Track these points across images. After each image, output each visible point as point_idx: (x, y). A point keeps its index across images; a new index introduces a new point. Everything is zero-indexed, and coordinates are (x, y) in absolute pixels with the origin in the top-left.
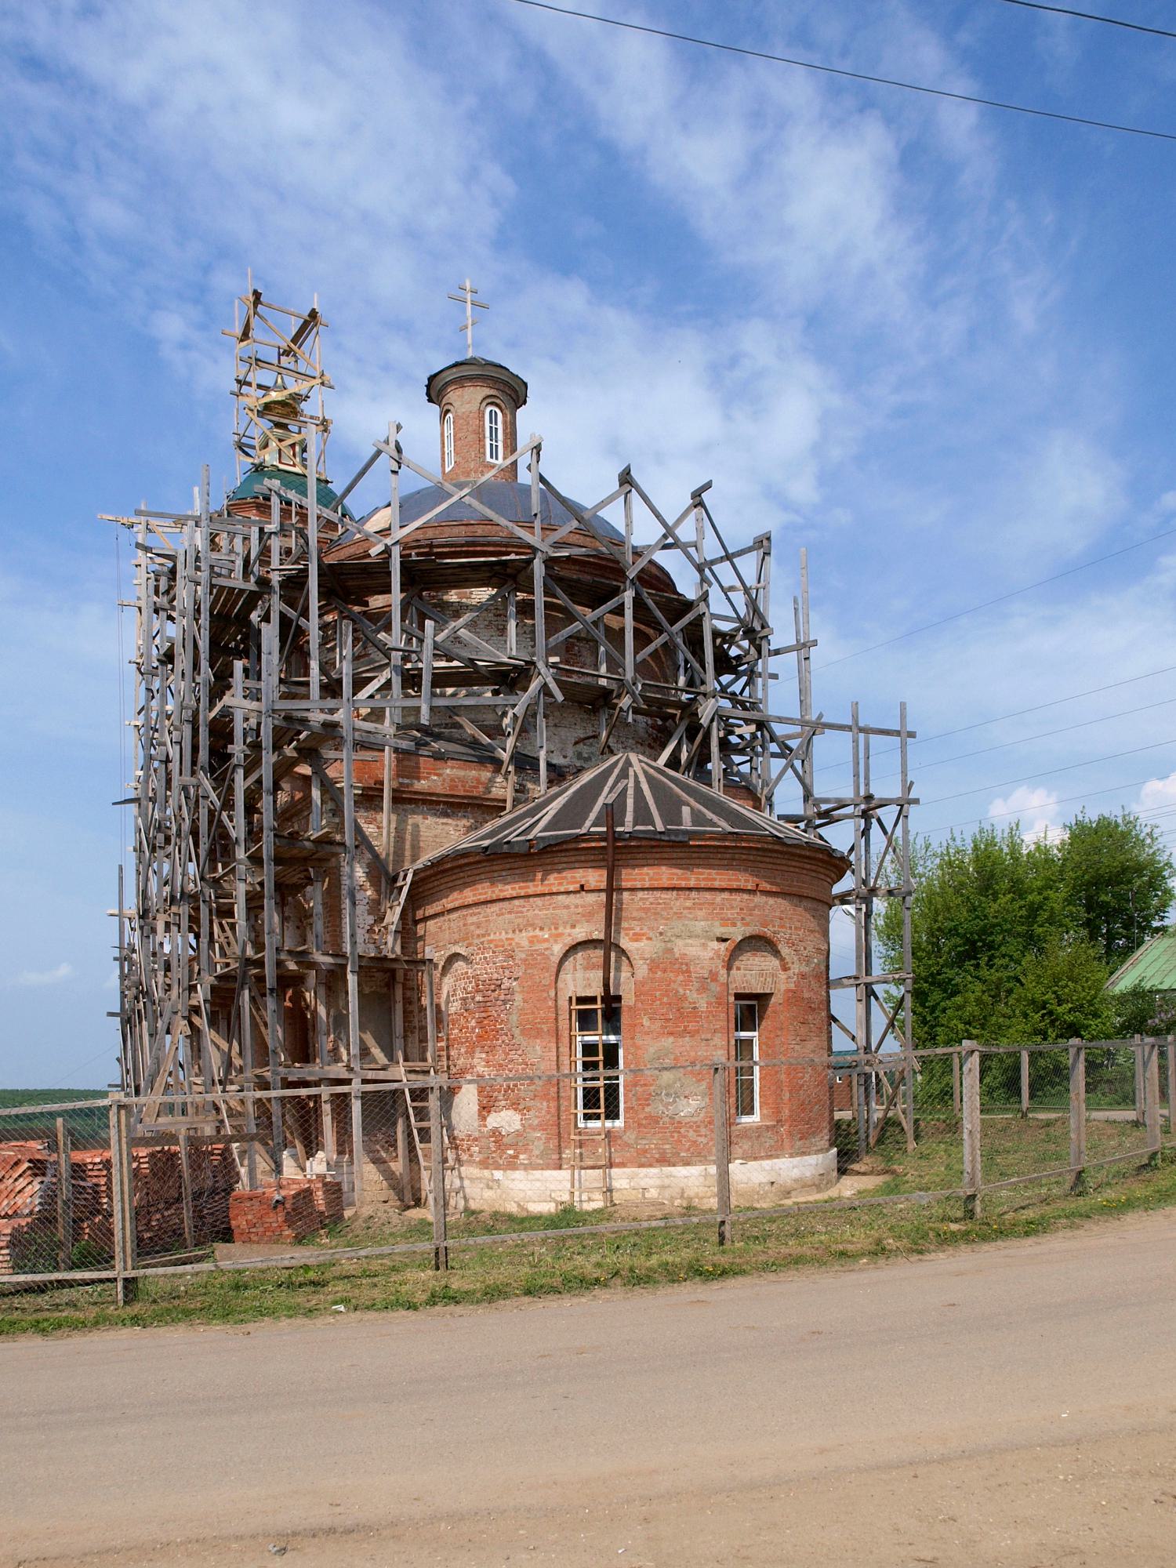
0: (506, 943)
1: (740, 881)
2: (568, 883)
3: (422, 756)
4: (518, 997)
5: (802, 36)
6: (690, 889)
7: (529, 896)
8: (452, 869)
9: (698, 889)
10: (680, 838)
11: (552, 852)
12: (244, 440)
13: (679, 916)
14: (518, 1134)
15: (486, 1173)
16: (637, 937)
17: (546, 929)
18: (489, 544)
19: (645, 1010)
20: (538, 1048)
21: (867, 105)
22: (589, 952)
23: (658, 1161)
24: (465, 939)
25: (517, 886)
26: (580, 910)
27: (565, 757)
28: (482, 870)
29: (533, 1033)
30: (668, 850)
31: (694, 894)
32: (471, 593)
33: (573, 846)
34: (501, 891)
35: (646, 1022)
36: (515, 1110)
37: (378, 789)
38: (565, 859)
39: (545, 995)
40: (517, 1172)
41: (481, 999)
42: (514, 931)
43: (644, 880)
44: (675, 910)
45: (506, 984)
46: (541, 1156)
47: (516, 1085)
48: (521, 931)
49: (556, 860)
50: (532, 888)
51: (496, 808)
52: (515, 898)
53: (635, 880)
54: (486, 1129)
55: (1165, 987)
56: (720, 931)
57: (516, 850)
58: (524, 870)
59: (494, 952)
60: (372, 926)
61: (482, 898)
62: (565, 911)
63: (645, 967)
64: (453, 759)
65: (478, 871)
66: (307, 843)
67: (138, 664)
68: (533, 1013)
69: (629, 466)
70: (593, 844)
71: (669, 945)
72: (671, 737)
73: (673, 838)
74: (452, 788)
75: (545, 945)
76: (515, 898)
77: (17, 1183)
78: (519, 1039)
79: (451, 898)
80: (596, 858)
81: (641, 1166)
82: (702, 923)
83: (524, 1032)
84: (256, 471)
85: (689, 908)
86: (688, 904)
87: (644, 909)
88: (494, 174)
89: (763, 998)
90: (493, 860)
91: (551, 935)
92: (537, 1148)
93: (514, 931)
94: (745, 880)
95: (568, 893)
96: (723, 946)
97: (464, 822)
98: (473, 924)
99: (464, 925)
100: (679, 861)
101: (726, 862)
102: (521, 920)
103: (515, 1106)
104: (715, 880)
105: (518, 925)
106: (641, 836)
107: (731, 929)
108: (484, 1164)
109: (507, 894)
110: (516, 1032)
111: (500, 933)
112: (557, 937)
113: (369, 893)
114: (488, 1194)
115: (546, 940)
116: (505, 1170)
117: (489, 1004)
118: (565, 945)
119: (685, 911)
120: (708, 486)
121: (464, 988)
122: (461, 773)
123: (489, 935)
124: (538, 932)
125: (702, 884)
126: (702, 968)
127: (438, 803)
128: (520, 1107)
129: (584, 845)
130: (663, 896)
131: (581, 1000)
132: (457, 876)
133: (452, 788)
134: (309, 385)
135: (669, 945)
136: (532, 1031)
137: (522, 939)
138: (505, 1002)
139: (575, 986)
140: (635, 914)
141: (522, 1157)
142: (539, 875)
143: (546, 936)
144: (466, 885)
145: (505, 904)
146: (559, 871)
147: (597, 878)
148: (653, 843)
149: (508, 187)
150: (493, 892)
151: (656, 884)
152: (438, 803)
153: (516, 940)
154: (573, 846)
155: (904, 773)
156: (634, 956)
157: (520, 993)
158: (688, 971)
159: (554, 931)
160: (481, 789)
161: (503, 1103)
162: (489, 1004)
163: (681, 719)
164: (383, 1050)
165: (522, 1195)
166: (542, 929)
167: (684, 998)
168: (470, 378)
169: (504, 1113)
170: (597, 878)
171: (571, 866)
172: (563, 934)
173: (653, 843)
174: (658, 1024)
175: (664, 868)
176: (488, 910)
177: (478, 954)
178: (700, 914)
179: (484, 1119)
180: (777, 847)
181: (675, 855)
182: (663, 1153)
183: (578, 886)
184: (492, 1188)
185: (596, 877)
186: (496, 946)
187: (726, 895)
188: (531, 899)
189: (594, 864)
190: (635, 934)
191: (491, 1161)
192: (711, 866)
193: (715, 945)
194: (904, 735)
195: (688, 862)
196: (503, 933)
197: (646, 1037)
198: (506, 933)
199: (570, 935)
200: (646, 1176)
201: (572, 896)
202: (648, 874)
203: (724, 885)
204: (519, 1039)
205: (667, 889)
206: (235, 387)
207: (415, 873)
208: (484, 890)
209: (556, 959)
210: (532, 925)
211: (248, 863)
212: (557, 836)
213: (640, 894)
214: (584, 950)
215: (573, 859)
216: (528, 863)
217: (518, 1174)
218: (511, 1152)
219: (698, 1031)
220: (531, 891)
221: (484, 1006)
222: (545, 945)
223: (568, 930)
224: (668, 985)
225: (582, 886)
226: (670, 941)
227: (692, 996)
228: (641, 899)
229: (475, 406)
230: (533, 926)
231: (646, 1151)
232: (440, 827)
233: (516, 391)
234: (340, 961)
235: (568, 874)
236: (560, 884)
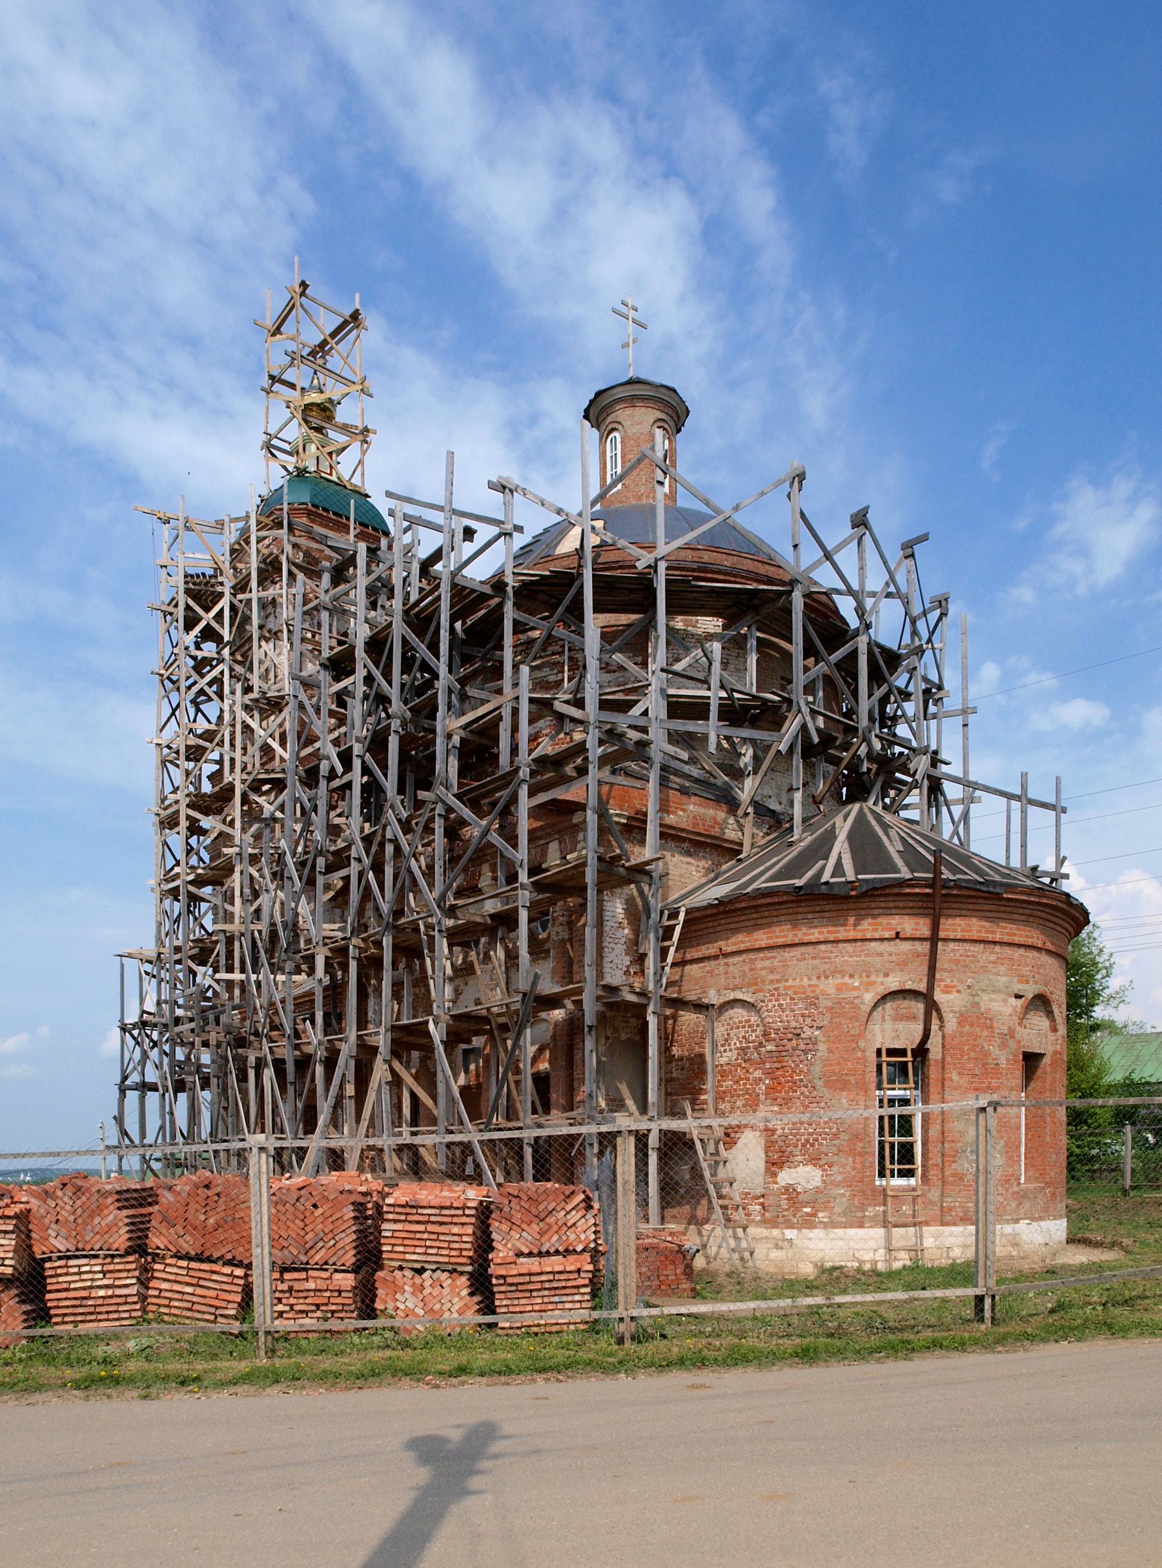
0: (809, 989)
1: (1032, 937)
2: (883, 930)
3: (672, 788)
4: (822, 1047)
5: (609, 93)
6: (994, 943)
7: (837, 941)
8: (744, 908)
9: (1001, 943)
10: (998, 890)
11: (872, 895)
12: (275, 442)
13: (985, 970)
14: (818, 1191)
15: (776, 1232)
16: (947, 990)
17: (856, 976)
18: (719, 572)
19: (954, 1064)
20: (844, 1101)
21: (671, 171)
22: (898, 1002)
23: (962, 1219)
24: (755, 984)
25: (825, 930)
26: (894, 958)
27: (780, 803)
28: (783, 912)
29: (839, 1085)
30: (982, 901)
31: (997, 948)
32: (697, 621)
33: (896, 890)
34: (805, 934)
35: (955, 1077)
36: (815, 1165)
37: (639, 819)
38: (883, 905)
39: (854, 1045)
40: (816, 1231)
41: (774, 1048)
42: (819, 978)
43: (956, 930)
44: (981, 964)
45: (808, 1032)
46: (844, 1214)
47: (817, 1140)
48: (827, 977)
49: (873, 905)
50: (842, 933)
51: (733, 851)
52: (821, 942)
53: (948, 930)
54: (776, 1186)
55: (1153, 1080)
56: (1018, 987)
57: (836, 891)
58: (834, 914)
59: (792, 999)
60: (628, 967)
61: (780, 941)
62: (878, 959)
63: (955, 1020)
64: (695, 795)
65: (779, 913)
66: (621, 870)
67: (162, 675)
68: (839, 1064)
69: (867, 508)
70: (917, 890)
71: (976, 999)
72: (869, 794)
73: (991, 889)
74: (695, 825)
75: (855, 993)
76: (821, 942)
77: (568, 1217)
78: (822, 1090)
79: (730, 941)
80: (916, 904)
81: (943, 1224)
82: (1004, 978)
83: (828, 1084)
84: (298, 476)
85: (994, 963)
86: (993, 958)
87: (954, 960)
88: (291, 186)
89: (1040, 1056)
90: (802, 901)
91: (861, 983)
92: (840, 1206)
93: (819, 978)
94: (1035, 937)
95: (882, 940)
96: (1020, 1002)
97: (703, 863)
98: (763, 968)
99: (751, 970)
100: (988, 914)
101: (1024, 918)
102: (827, 966)
103: (814, 1161)
104: (1015, 935)
105: (824, 971)
106: (964, 885)
107: (1026, 987)
108: (772, 1223)
109: (813, 938)
110: (819, 1083)
111: (802, 980)
112: (868, 985)
113: (626, 931)
114: (775, 1254)
115: (857, 988)
116: (799, 1228)
117: (784, 1054)
118: (877, 993)
119: (991, 965)
120: (924, 538)
121: (744, 1037)
122: (702, 811)
123: (787, 981)
124: (847, 980)
125: (1006, 939)
126: (1003, 1024)
127: (684, 840)
128: (821, 1163)
129: (908, 890)
130: (972, 948)
131: (891, 1052)
132: (750, 916)
133: (695, 825)
134: (346, 390)
135: (976, 999)
136: (838, 1083)
137: (829, 986)
138: (805, 1052)
139: (883, 1038)
140: (946, 966)
141: (820, 1215)
142: (852, 920)
143: (857, 984)
144: (757, 927)
145: (810, 949)
146: (874, 917)
147: (913, 926)
148: (972, 893)
149: (308, 205)
150: (795, 935)
151: (967, 935)
152: (684, 840)
153: (822, 987)
154: (896, 890)
155: (1058, 847)
156: (944, 1009)
157: (825, 1042)
158: (992, 1027)
159: (865, 979)
160: (717, 830)
161: (799, 1158)
162: (784, 1054)
163: (877, 774)
164: (635, 1102)
165: (820, 1255)
166: (851, 976)
167: (987, 1054)
168: (642, 398)
169: (800, 1169)
170: (913, 926)
171: (888, 912)
172: (875, 983)
173: (972, 893)
174: (966, 1079)
175: (974, 920)
176: (786, 954)
177: (770, 1001)
178: (1002, 969)
179: (775, 1175)
180: (1064, 906)
181: (986, 907)
182: (966, 1212)
183: (893, 933)
184: (782, 1248)
185: (915, 925)
186: (796, 993)
187: (1021, 951)
188: (840, 945)
189: (910, 911)
190: (946, 986)
191: (781, 1220)
192: (1013, 921)
193: (1013, 1001)
194: (1059, 809)
195: (996, 915)
196: (805, 979)
197: (954, 1092)
198: (809, 979)
199: (882, 984)
200: (951, 1235)
201: (886, 943)
202: (960, 925)
203: (1022, 940)
204: (822, 1090)
205: (975, 941)
206: (266, 382)
207: (687, 912)
208: (783, 933)
209: (866, 1008)
210: (841, 972)
211: (531, 889)
212: (881, 880)
213: (952, 945)
214: (894, 1000)
215: (891, 904)
216: (840, 907)
217: (817, 1233)
218: (808, 1210)
219: (998, 1088)
220: (841, 936)
221: (779, 1055)
222: (855, 993)
223: (881, 979)
224: (975, 1040)
225: (897, 934)
226: (977, 995)
227: (995, 1052)
228: (953, 950)
229: (645, 428)
230: (842, 973)
231: (950, 1209)
232: (685, 866)
233: (679, 418)
234: (643, 1001)
235: (883, 920)
236: (875, 930)
